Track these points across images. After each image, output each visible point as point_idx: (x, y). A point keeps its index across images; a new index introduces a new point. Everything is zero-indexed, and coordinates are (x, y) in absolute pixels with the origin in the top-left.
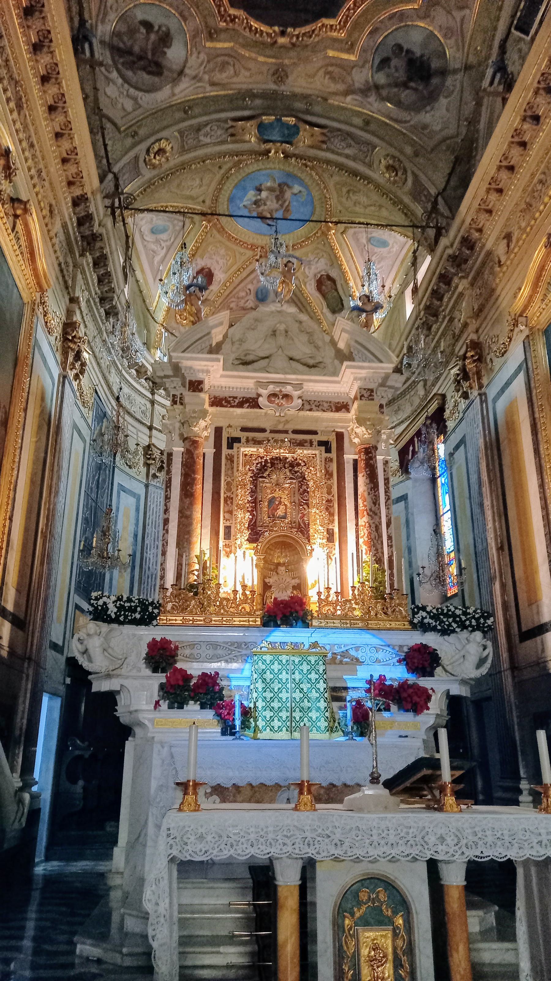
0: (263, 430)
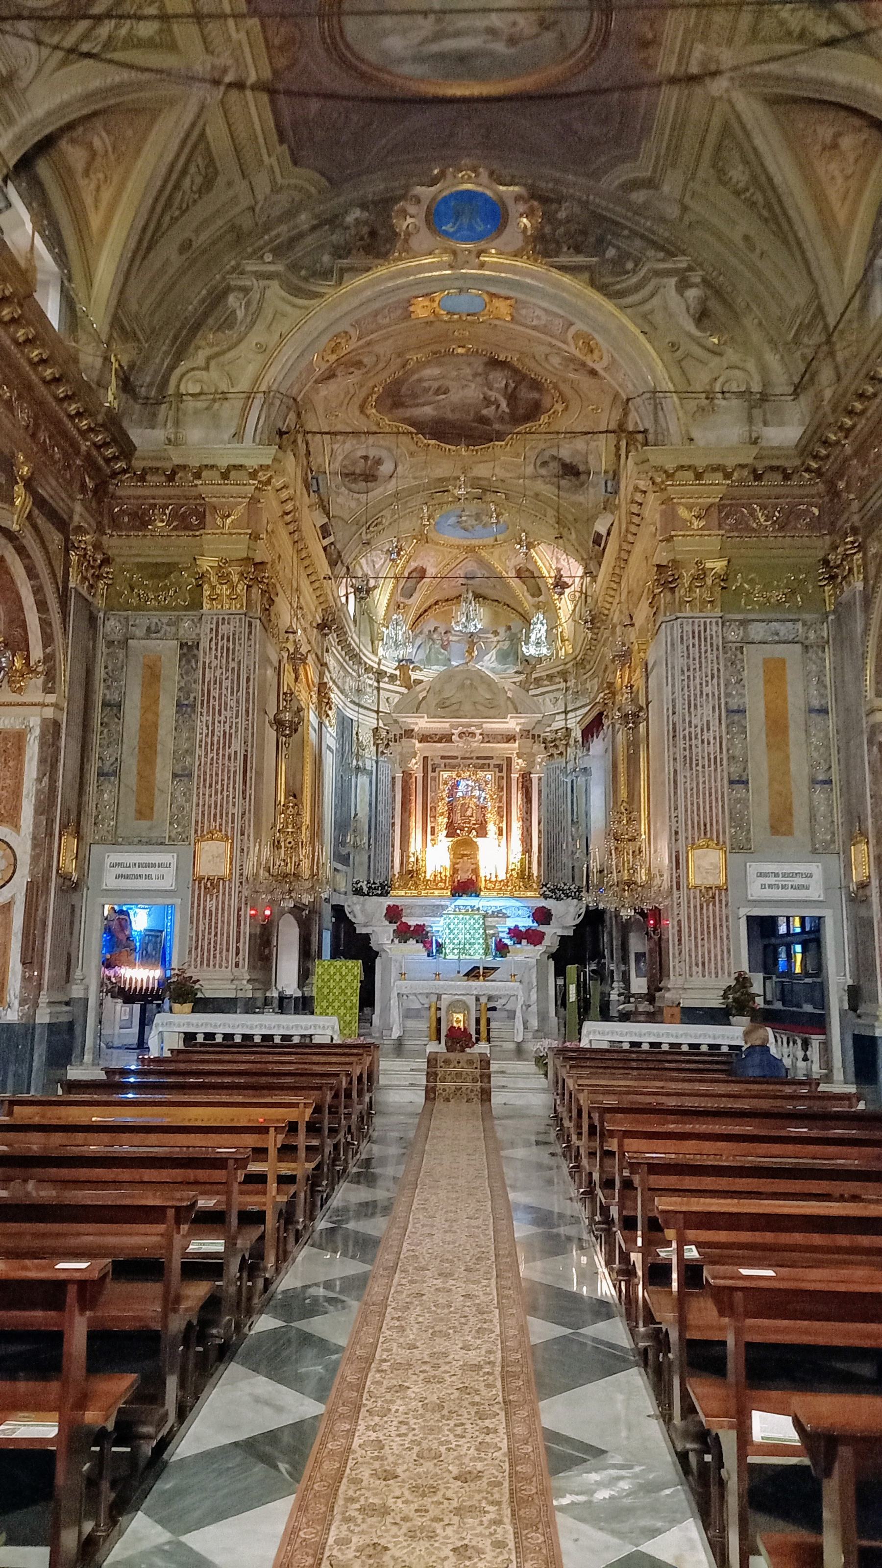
0: (456, 758)
